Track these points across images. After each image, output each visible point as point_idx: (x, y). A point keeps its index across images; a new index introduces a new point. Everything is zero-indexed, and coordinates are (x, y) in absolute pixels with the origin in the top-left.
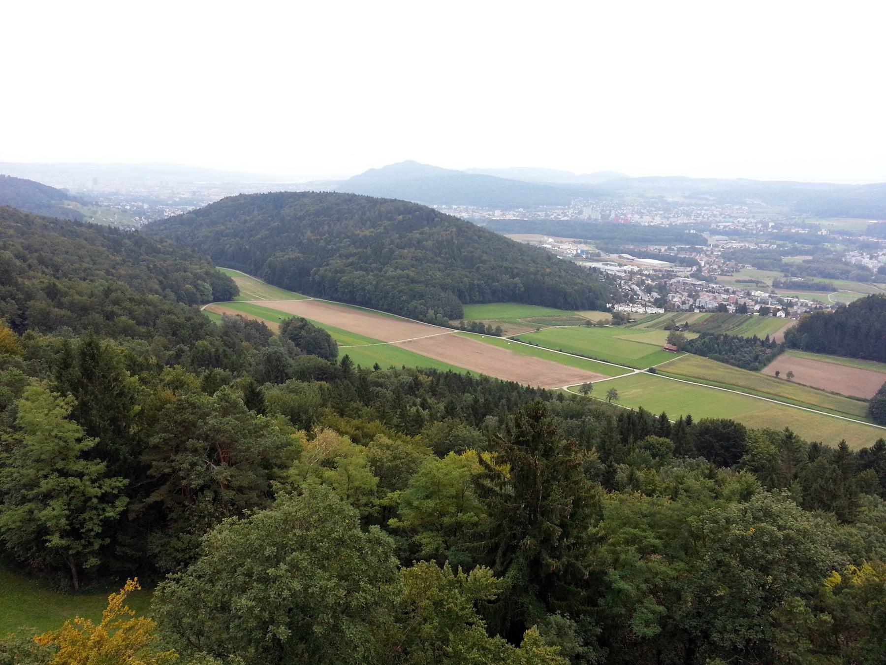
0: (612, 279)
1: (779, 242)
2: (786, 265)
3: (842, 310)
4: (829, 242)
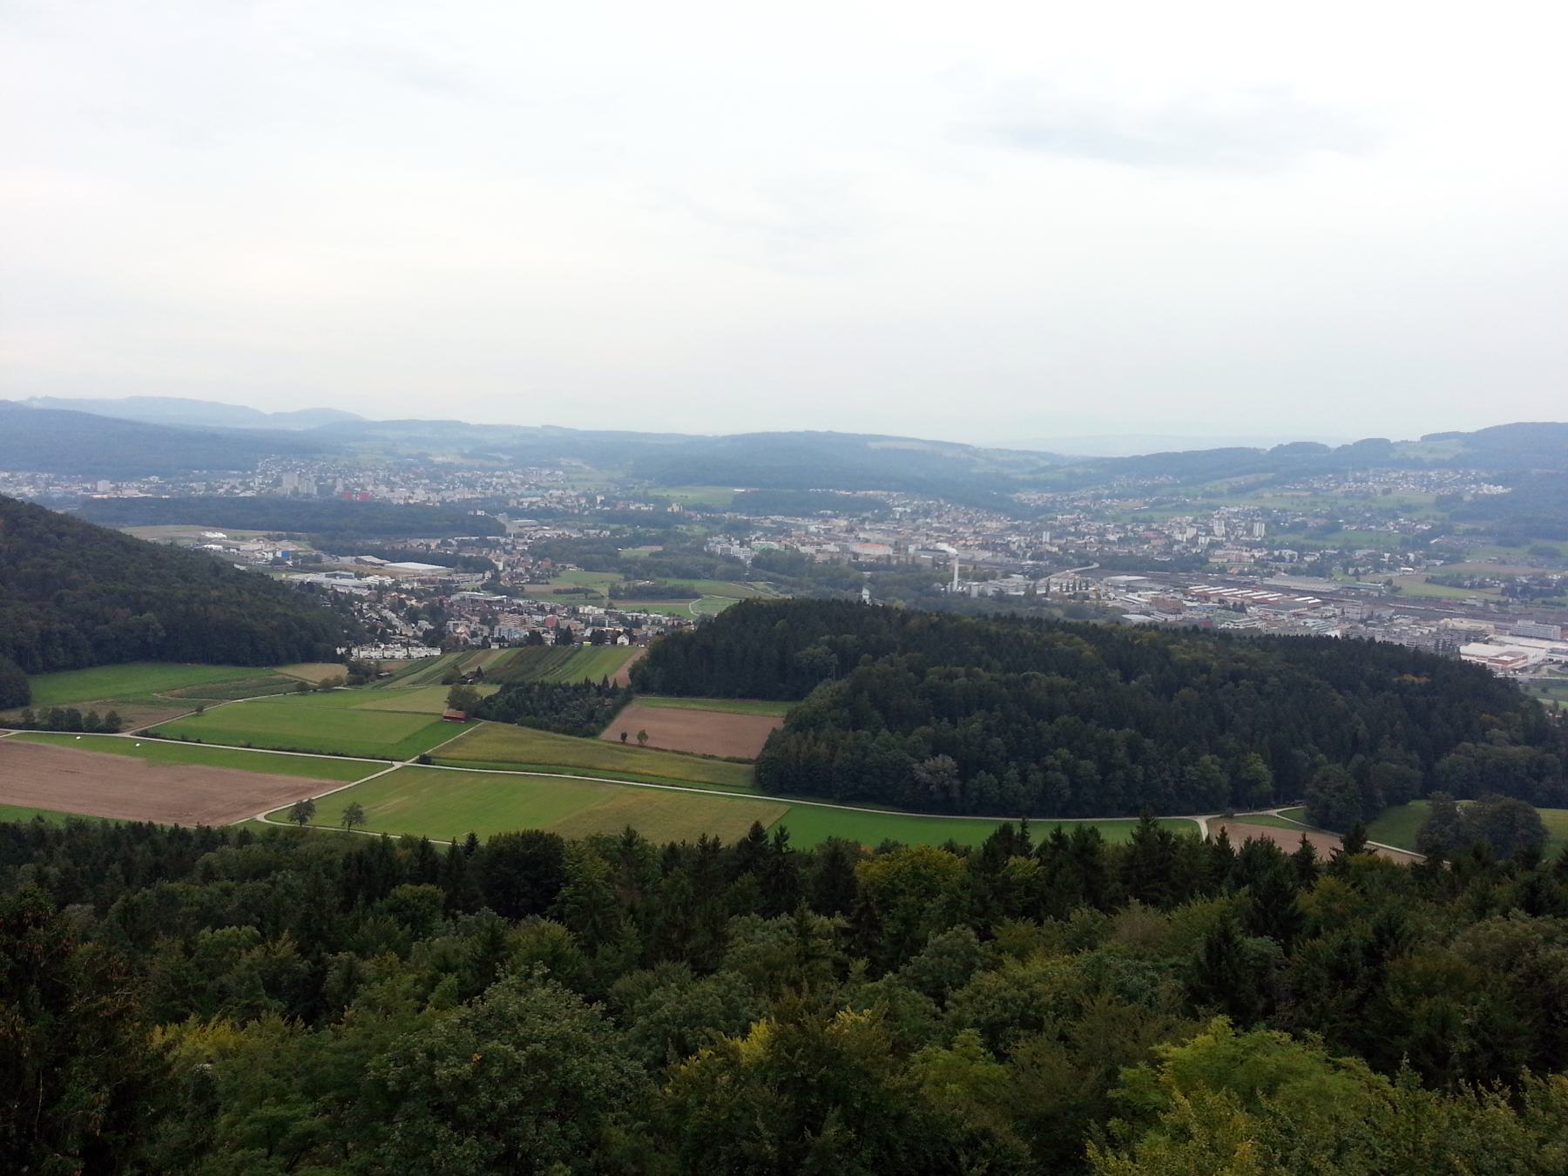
0: (344, 602)
2: (627, 561)
3: (706, 625)
4: (683, 524)
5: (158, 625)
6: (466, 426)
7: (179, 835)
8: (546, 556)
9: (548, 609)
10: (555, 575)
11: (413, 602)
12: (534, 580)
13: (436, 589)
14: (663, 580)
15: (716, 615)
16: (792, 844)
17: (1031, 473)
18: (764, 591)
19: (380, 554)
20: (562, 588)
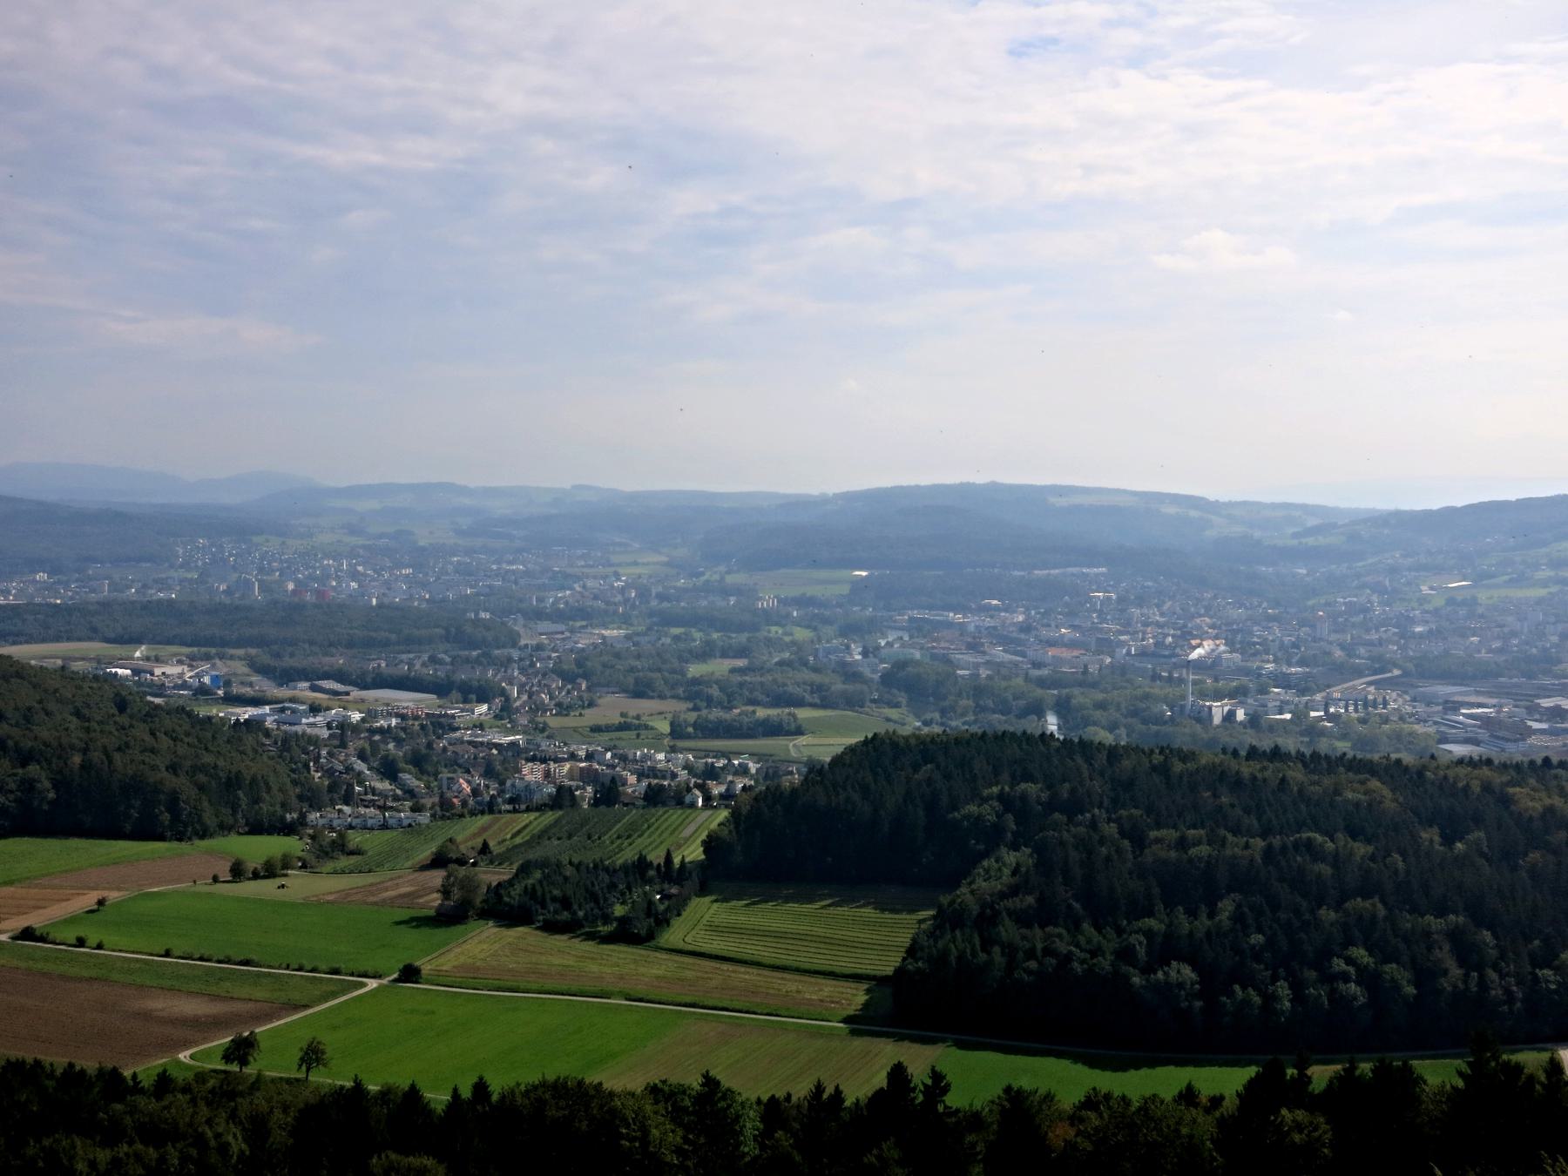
0: (293, 747)
1: (676, 631)
2: (696, 681)
3: (815, 772)
4: (776, 624)
5: (47, 784)
6: (463, 491)
7: (73, 1077)
8: (578, 676)
9: (582, 754)
10: (591, 704)
11: (391, 746)
12: (563, 709)
13: (423, 727)
14: (751, 708)
15: (828, 759)
16: (954, 1100)
17: (1295, 535)
18: (908, 722)
19: (340, 677)
20: (602, 722)
